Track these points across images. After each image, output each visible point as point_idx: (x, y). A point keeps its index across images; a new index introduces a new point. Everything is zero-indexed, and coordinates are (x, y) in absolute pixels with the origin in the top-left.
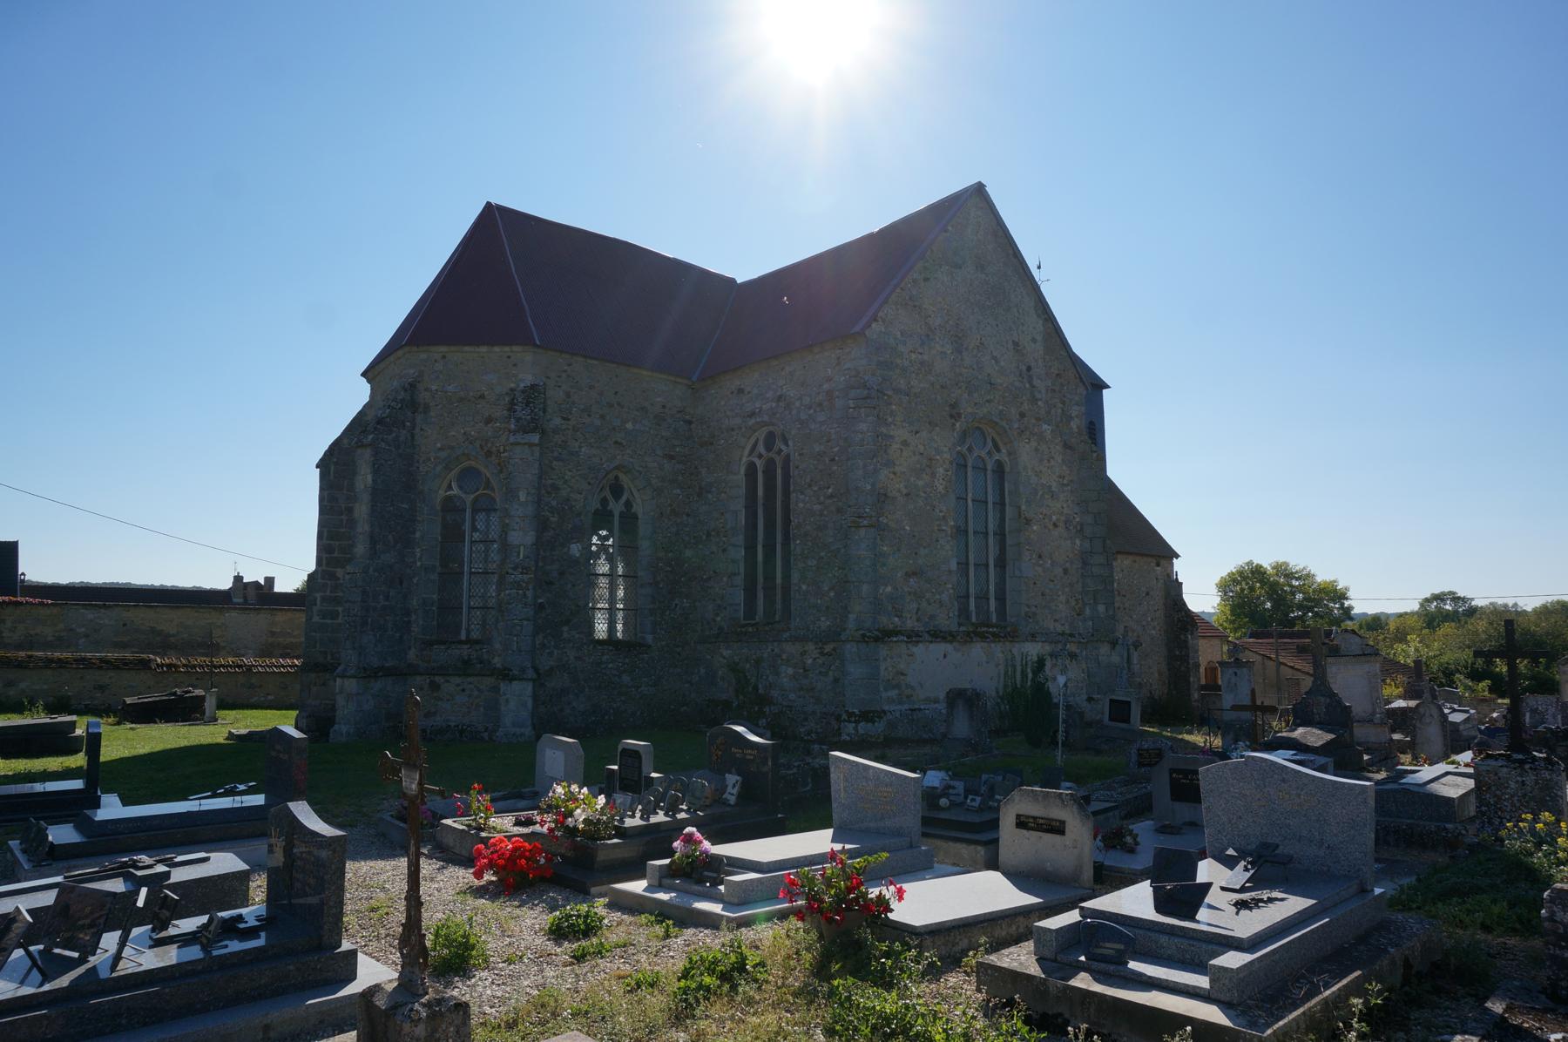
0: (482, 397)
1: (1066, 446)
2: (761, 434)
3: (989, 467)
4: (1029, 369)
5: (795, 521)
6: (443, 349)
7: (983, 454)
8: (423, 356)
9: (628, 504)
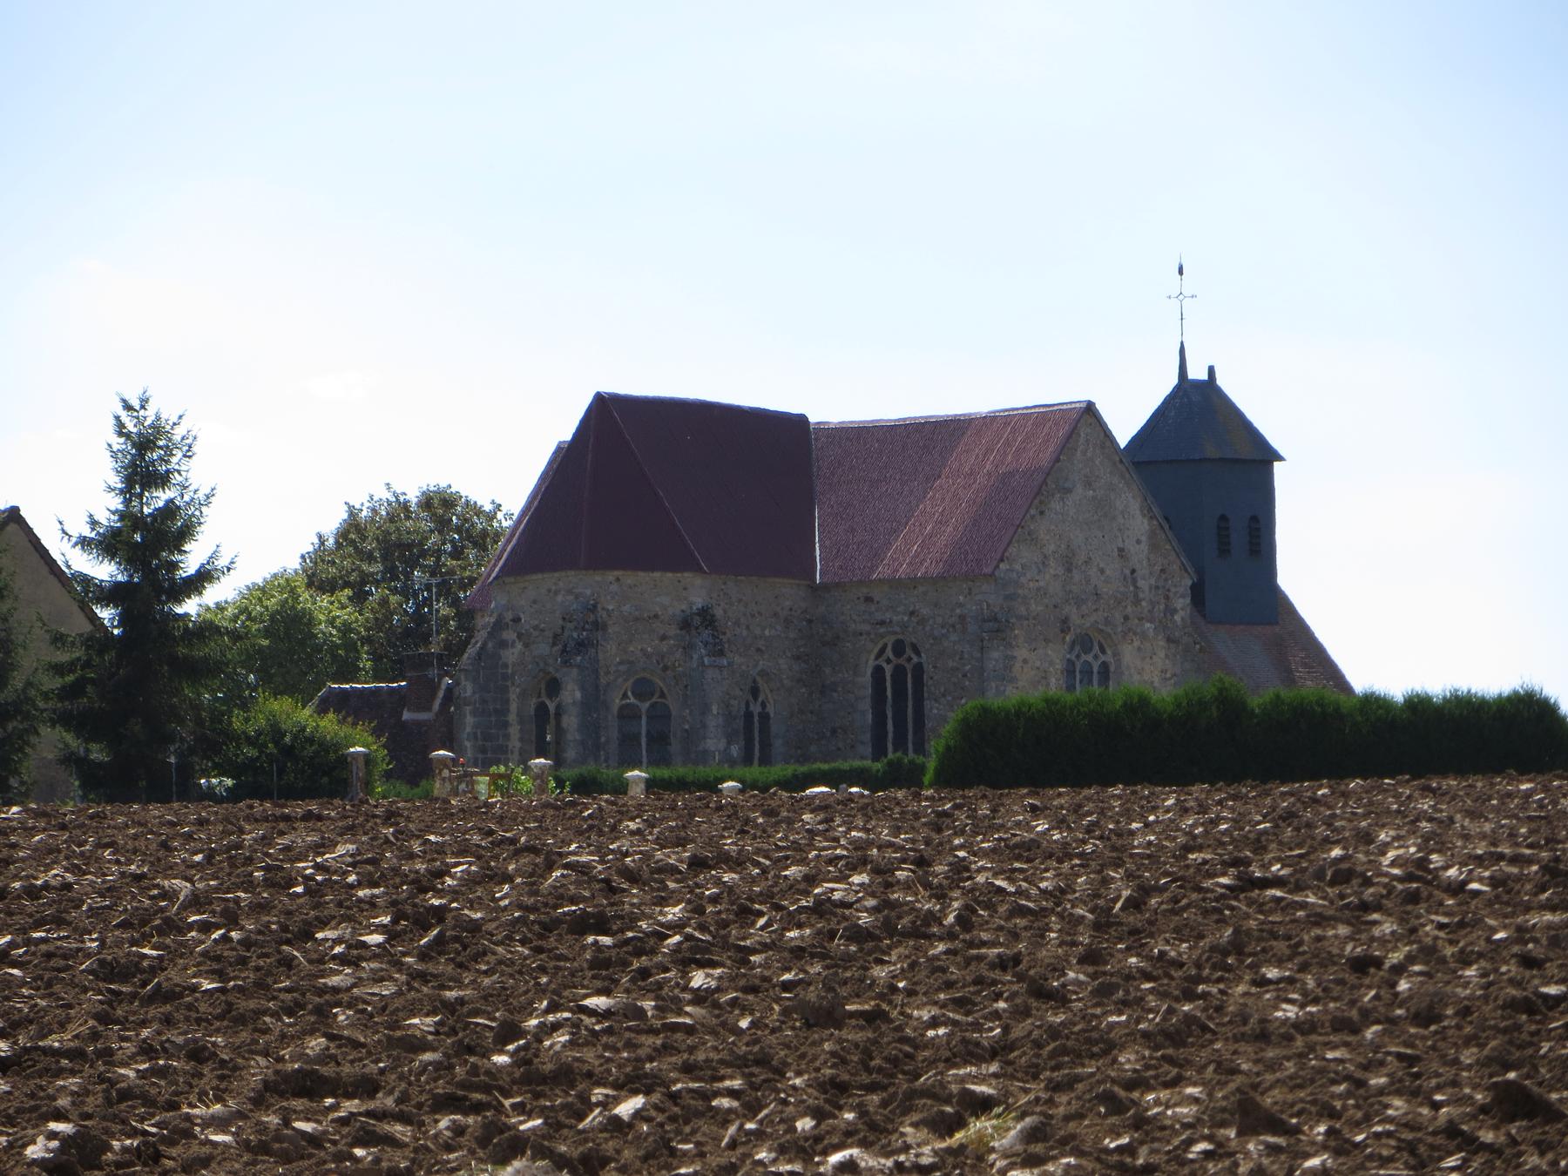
0: (656, 616)
1: (1169, 640)
2: (890, 640)
3: (1095, 670)
4: (1133, 571)
5: (929, 725)
6: (617, 573)
7: (1089, 658)
8: (598, 578)
9: (763, 705)
